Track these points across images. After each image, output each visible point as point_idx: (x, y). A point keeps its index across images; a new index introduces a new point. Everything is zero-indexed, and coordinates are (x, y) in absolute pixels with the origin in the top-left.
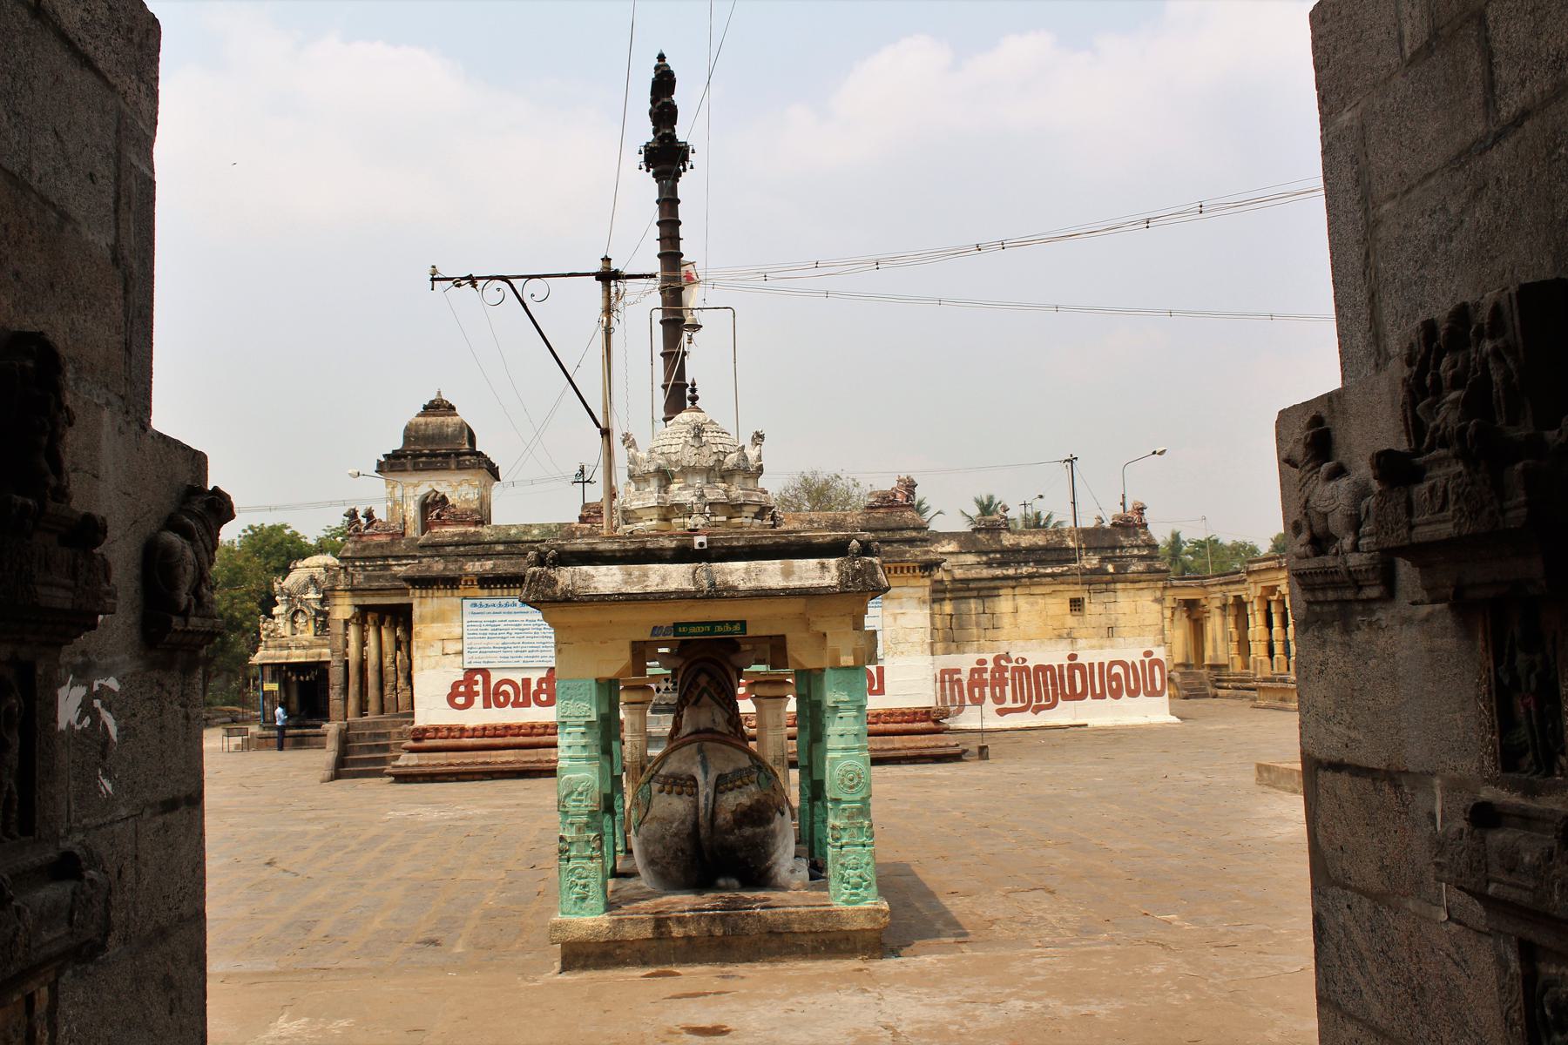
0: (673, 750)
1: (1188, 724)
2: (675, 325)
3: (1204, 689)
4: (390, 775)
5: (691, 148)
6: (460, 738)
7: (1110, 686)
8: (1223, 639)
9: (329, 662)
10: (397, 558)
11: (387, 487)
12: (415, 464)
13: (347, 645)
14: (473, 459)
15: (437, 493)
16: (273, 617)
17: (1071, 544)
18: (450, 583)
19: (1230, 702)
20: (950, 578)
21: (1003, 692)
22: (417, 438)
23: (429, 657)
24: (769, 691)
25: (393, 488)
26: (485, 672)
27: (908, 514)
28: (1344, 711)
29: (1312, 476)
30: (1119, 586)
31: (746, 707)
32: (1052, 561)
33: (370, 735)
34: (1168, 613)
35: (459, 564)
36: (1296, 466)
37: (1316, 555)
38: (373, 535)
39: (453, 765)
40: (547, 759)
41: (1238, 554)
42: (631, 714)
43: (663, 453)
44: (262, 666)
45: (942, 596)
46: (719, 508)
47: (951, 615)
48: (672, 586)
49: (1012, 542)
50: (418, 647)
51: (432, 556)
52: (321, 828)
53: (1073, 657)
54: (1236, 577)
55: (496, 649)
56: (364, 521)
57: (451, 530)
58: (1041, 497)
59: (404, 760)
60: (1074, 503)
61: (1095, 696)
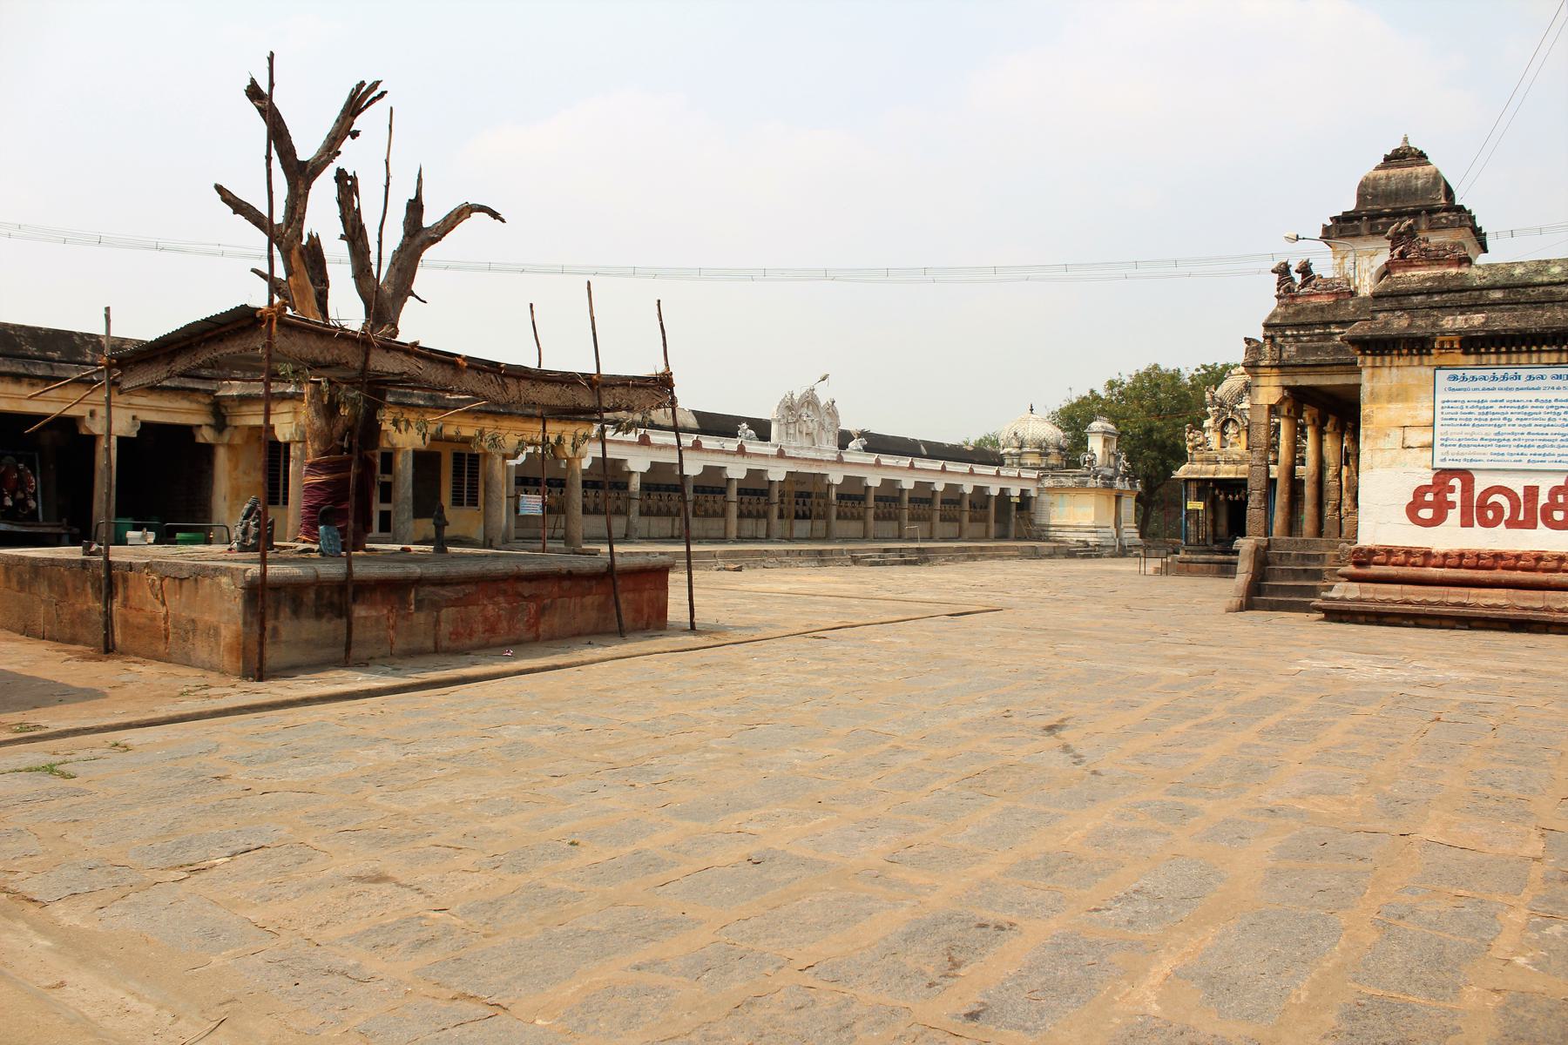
6: (1423, 566)
12: (1372, 226)
18: (1418, 346)
22: (1375, 196)
25: (1343, 258)
26: (1466, 475)
33: (1297, 556)
38: (1310, 295)
39: (1411, 603)
40: (1561, 606)
44: (1187, 481)
50: (1366, 437)
51: (1392, 310)
52: (1183, 672)
55: (1485, 442)
56: (1298, 278)
57: (1421, 273)
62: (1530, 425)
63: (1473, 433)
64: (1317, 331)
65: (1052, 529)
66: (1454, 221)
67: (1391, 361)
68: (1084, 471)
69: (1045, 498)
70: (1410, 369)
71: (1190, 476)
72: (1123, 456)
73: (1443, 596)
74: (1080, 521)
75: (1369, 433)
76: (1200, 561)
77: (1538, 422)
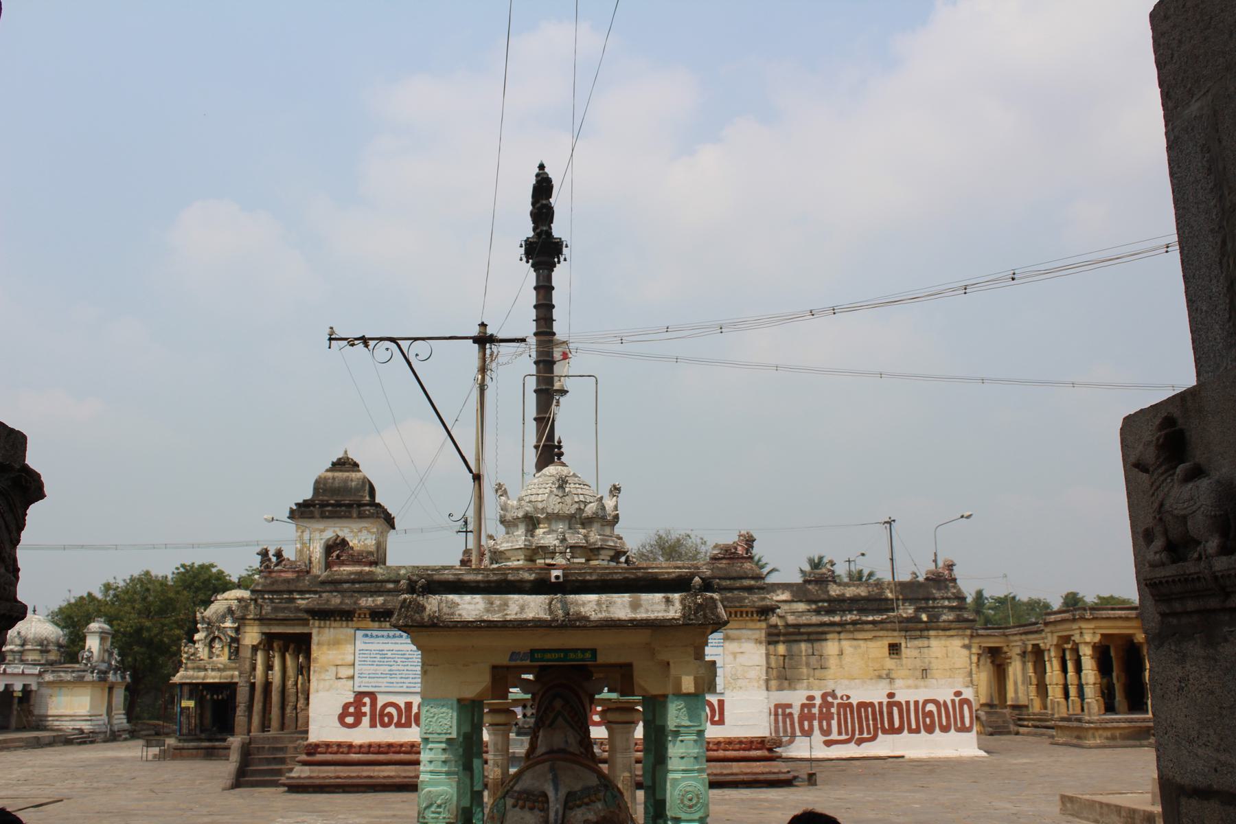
0: (528, 768)
1: (994, 758)
2: (547, 394)
3: (1008, 727)
4: (284, 785)
5: (565, 243)
6: (348, 753)
7: (924, 722)
8: (1023, 683)
9: (237, 683)
10: (301, 592)
11: (297, 531)
13: (254, 668)
14: (372, 510)
15: (338, 536)
16: (194, 642)
17: (890, 595)
18: (345, 615)
19: (1030, 739)
20: (783, 624)
21: (829, 725)
22: (325, 490)
23: (324, 680)
24: (618, 718)
25: (302, 532)
26: (372, 696)
27: (747, 565)
28: (1211, 732)
29: (1166, 479)
30: (932, 633)
31: (598, 732)
32: (873, 610)
33: (269, 748)
34: (975, 658)
35: (355, 599)
36: (1146, 470)
37: (1174, 562)
38: (281, 571)
39: (340, 778)
41: (1033, 609)
42: (495, 734)
43: (530, 502)
44: (182, 685)
45: (775, 639)
46: (579, 551)
47: (784, 656)
48: (530, 614)
49: (838, 592)
50: (315, 671)
51: (331, 592)
53: (891, 695)
54: (1034, 628)
56: (274, 559)
58: (863, 555)
59: (297, 772)
60: (892, 559)
61: (911, 731)
62: (407, 665)
63: (376, 670)
64: (285, 596)
65: (50, 719)
66: (373, 513)
67: (330, 624)
68: (82, 667)
69: (45, 691)
70: (342, 629)
71: (184, 681)
72: (116, 651)
73: (359, 772)
74: (76, 711)
75: (316, 669)
76: (190, 747)
77: (412, 663)
